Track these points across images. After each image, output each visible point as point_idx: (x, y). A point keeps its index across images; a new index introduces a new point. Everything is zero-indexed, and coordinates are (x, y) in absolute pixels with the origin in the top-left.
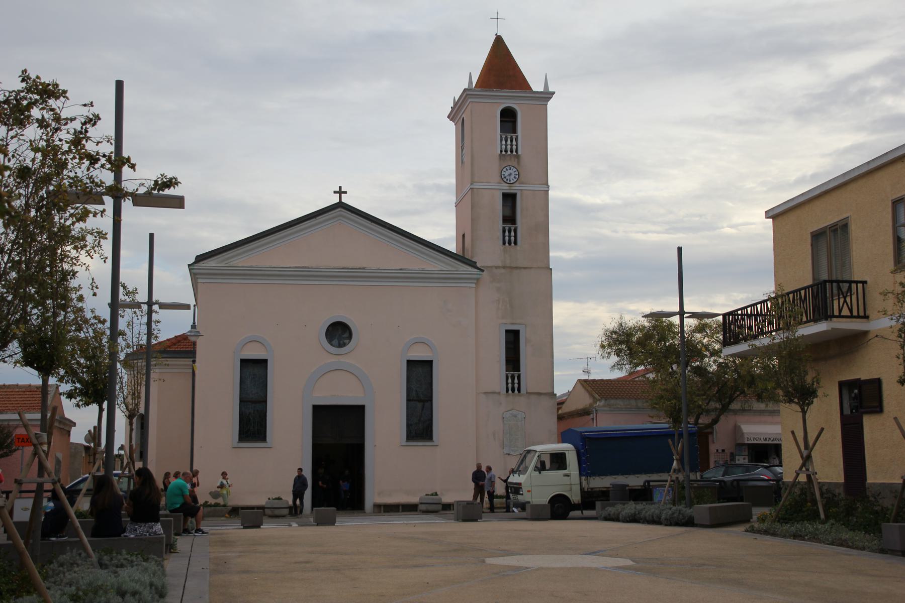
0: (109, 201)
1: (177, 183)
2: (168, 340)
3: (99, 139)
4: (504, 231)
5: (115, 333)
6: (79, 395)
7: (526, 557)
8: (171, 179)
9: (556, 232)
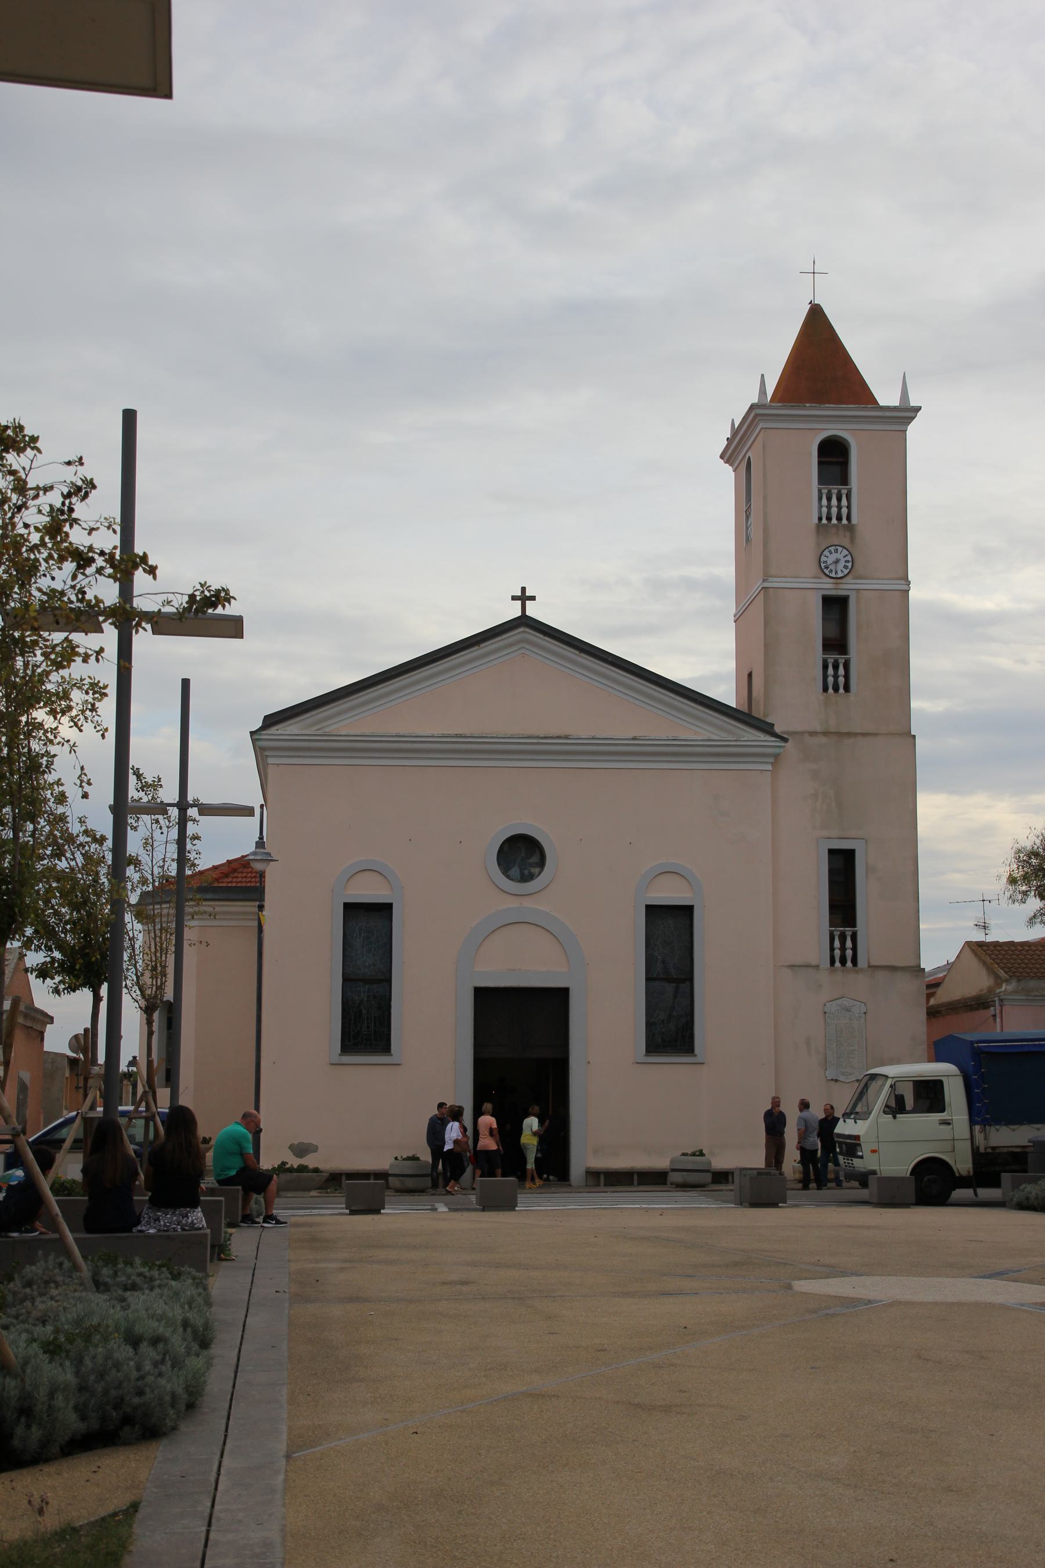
0: (109, 637)
1: (228, 599)
2: (215, 868)
3: (94, 526)
4: (825, 667)
5: (121, 859)
6: (58, 973)
7: (868, 1280)
8: (218, 592)
9: (921, 662)
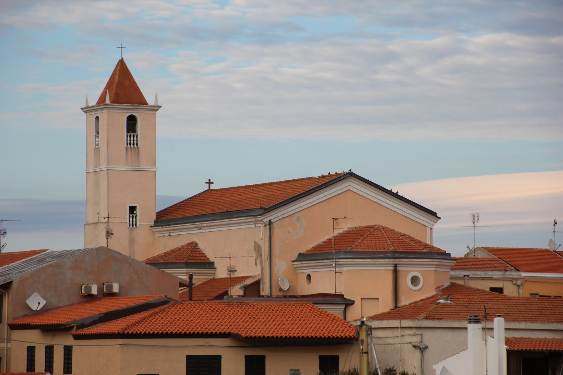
4: (130, 217)
